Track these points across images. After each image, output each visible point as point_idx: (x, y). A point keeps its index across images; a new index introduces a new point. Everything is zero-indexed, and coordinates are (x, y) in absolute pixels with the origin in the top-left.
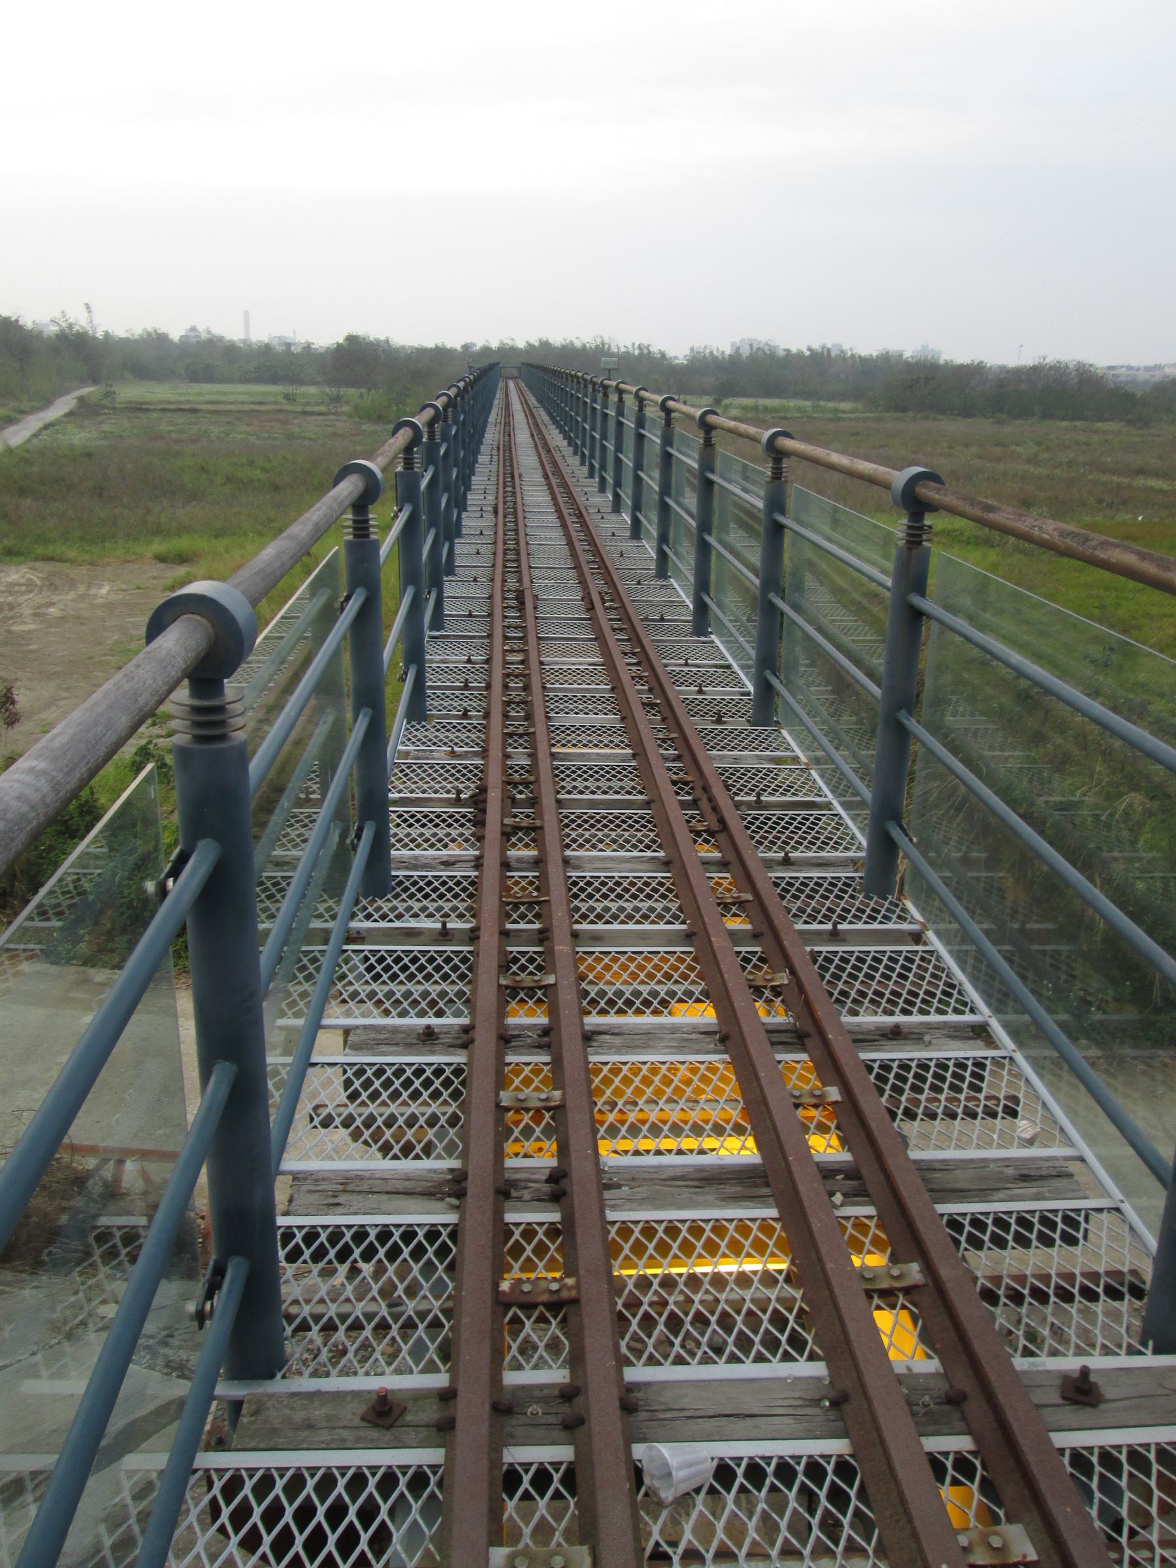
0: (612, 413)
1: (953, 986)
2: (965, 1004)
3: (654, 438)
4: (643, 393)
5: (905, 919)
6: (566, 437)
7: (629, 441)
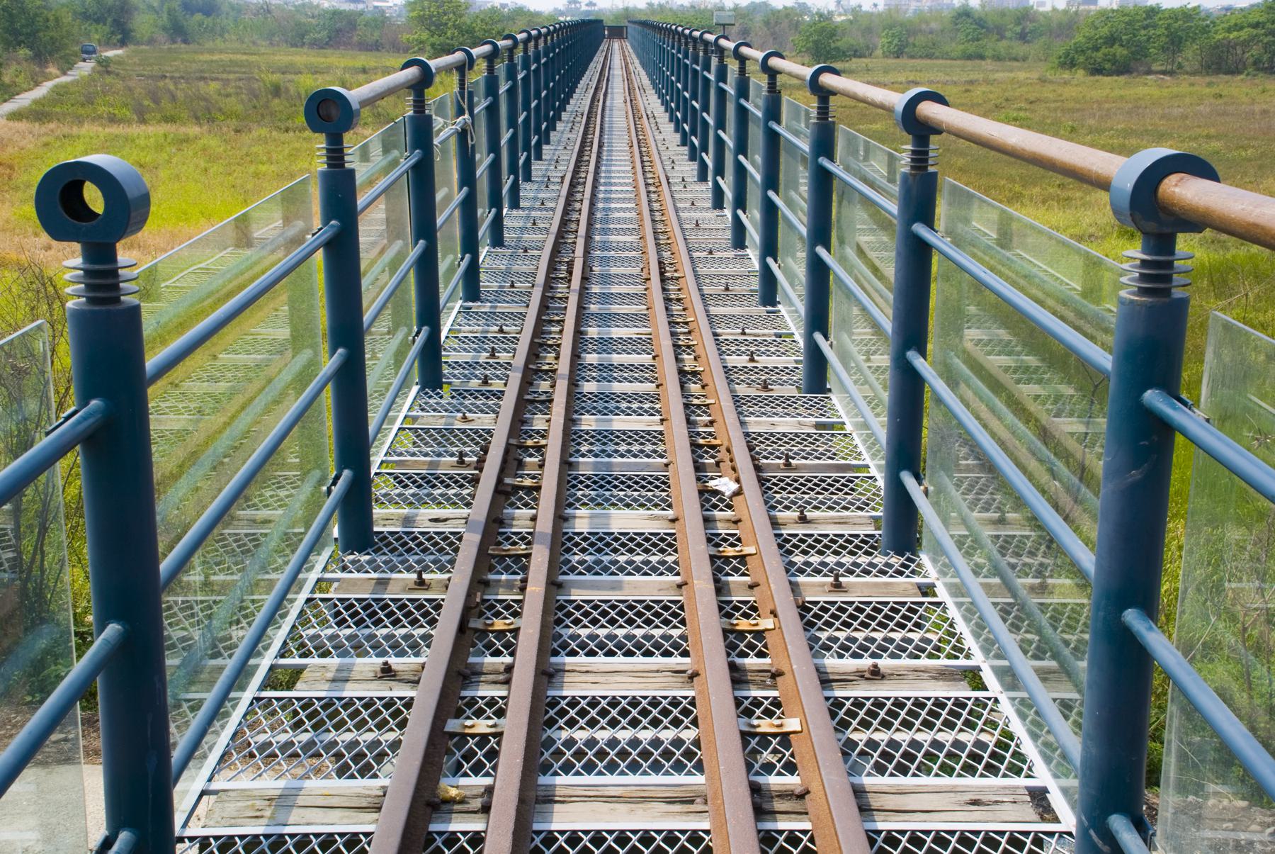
0: (730, 89)
1: (953, 635)
2: (961, 650)
3: (756, 109)
4: (774, 62)
5: (1018, 772)
6: (665, 104)
7: (756, 136)
